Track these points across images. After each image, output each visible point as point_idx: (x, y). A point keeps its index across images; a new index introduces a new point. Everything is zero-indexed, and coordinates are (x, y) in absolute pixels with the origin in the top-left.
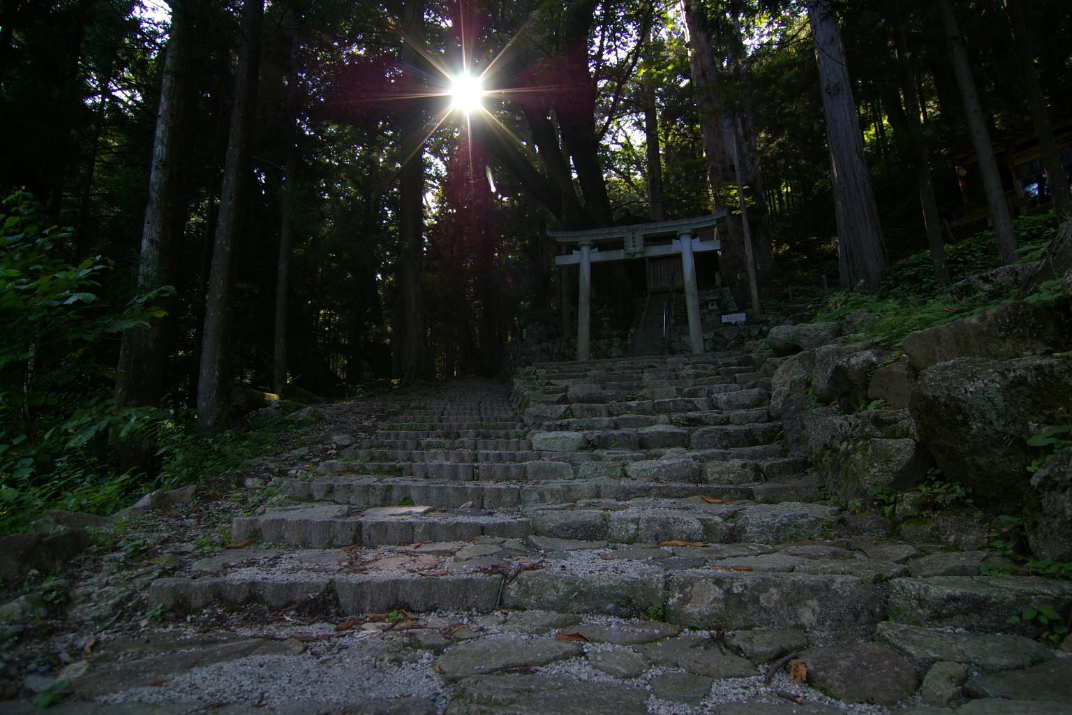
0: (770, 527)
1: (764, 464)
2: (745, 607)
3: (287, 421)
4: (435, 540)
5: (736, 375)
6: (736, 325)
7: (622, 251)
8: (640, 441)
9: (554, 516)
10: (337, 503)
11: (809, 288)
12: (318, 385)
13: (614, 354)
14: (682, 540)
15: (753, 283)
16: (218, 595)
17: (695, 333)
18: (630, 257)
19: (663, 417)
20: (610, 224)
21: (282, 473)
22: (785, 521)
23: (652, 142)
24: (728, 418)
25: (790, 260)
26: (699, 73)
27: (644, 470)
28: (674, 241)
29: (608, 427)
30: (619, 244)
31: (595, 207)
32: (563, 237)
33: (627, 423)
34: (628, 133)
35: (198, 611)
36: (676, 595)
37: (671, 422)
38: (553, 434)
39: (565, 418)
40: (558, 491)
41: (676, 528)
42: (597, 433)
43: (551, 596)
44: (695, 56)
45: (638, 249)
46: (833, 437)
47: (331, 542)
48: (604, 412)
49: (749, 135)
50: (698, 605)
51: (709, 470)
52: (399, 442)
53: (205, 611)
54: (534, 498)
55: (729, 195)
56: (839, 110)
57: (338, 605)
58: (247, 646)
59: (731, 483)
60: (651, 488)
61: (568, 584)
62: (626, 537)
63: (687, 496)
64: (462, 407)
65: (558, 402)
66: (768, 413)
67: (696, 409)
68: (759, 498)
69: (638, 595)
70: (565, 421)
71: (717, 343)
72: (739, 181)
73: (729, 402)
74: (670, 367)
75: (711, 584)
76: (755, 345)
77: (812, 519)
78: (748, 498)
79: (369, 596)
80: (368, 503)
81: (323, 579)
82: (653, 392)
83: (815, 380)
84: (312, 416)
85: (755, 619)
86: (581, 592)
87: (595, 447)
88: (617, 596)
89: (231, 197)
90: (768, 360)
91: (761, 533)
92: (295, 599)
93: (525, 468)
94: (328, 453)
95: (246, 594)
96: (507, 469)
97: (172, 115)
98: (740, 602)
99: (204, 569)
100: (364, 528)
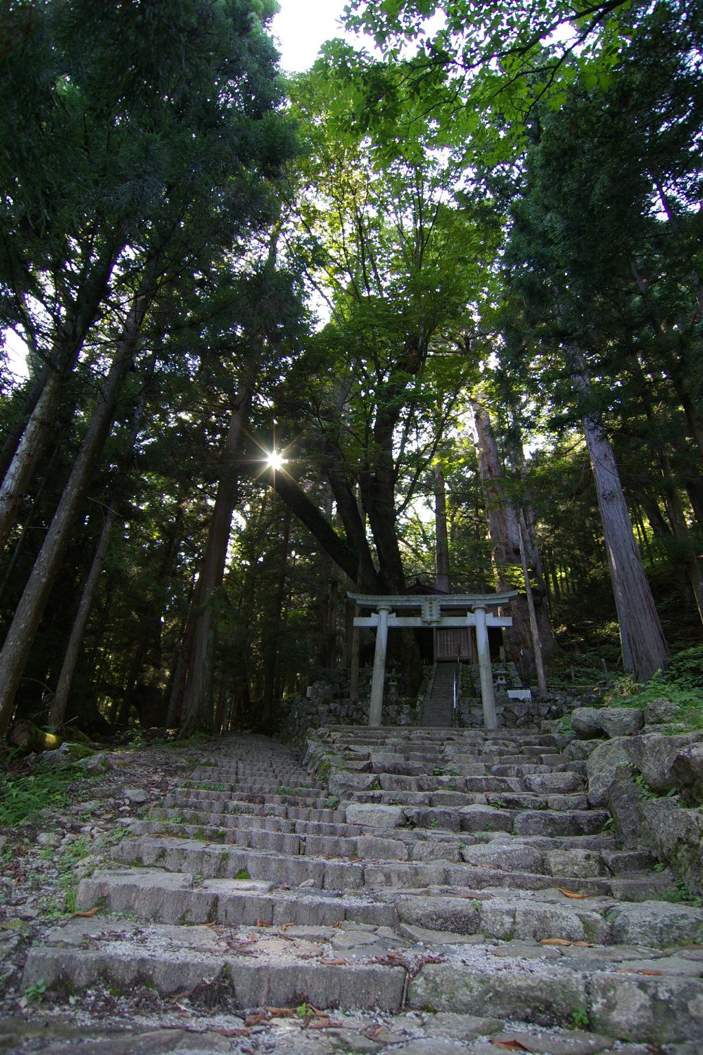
0: (653, 928)
1: (609, 856)
2: (675, 1016)
3: (74, 768)
4: (296, 922)
5: (543, 755)
6: (523, 701)
7: (419, 619)
8: (461, 821)
9: (420, 904)
10: (168, 870)
11: (589, 670)
12: (104, 733)
13: (403, 722)
14: (561, 937)
15: (539, 661)
16: (104, 973)
17: (489, 709)
18: (426, 625)
19: (480, 796)
20: (404, 591)
21: (76, 830)
22: (667, 922)
23: (440, 521)
24: (547, 803)
25: (573, 640)
26: (487, 468)
27: (483, 855)
28: (469, 614)
29: (422, 803)
30: (416, 612)
31: (389, 576)
32: (363, 600)
33: (442, 800)
34: (419, 512)
35: (82, 992)
36: (599, 999)
37: (488, 803)
38: (368, 806)
39: (373, 789)
40: (406, 873)
41: (554, 924)
42: (416, 809)
43: (464, 996)
44: (483, 455)
45: (435, 618)
46: (689, 831)
47: (183, 917)
48: (414, 786)
49: (531, 525)
50: (624, 1013)
51: (552, 860)
52: (205, 803)
53: (89, 992)
54: (379, 880)
55: (512, 576)
56: (614, 512)
57: (234, 996)
58: (168, 1037)
59: (576, 876)
60: (505, 876)
61: (482, 981)
62: (502, 932)
63: (542, 888)
64: (256, 768)
65: (363, 770)
66: (588, 800)
67: (510, 790)
68: (618, 895)
69: (558, 998)
70: (377, 792)
71: (507, 720)
72: (524, 564)
73: (543, 784)
74: (469, 740)
75: (635, 988)
76: (552, 725)
77: (693, 920)
78: (606, 894)
79: (266, 985)
80: (201, 873)
81: (217, 961)
82: (461, 768)
83: (647, 768)
84: (103, 765)
85: (686, 1030)
86: (497, 993)
87: (413, 825)
88: (536, 999)
89: (59, 532)
90: (573, 742)
91: (644, 934)
92: (185, 984)
93: (355, 844)
94: (121, 809)
95: (135, 974)
96: (337, 843)
97: (29, 455)
98: (669, 1010)
99: (65, 940)
100: (220, 903)
